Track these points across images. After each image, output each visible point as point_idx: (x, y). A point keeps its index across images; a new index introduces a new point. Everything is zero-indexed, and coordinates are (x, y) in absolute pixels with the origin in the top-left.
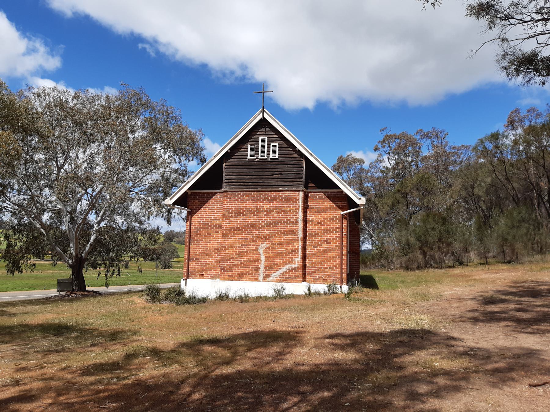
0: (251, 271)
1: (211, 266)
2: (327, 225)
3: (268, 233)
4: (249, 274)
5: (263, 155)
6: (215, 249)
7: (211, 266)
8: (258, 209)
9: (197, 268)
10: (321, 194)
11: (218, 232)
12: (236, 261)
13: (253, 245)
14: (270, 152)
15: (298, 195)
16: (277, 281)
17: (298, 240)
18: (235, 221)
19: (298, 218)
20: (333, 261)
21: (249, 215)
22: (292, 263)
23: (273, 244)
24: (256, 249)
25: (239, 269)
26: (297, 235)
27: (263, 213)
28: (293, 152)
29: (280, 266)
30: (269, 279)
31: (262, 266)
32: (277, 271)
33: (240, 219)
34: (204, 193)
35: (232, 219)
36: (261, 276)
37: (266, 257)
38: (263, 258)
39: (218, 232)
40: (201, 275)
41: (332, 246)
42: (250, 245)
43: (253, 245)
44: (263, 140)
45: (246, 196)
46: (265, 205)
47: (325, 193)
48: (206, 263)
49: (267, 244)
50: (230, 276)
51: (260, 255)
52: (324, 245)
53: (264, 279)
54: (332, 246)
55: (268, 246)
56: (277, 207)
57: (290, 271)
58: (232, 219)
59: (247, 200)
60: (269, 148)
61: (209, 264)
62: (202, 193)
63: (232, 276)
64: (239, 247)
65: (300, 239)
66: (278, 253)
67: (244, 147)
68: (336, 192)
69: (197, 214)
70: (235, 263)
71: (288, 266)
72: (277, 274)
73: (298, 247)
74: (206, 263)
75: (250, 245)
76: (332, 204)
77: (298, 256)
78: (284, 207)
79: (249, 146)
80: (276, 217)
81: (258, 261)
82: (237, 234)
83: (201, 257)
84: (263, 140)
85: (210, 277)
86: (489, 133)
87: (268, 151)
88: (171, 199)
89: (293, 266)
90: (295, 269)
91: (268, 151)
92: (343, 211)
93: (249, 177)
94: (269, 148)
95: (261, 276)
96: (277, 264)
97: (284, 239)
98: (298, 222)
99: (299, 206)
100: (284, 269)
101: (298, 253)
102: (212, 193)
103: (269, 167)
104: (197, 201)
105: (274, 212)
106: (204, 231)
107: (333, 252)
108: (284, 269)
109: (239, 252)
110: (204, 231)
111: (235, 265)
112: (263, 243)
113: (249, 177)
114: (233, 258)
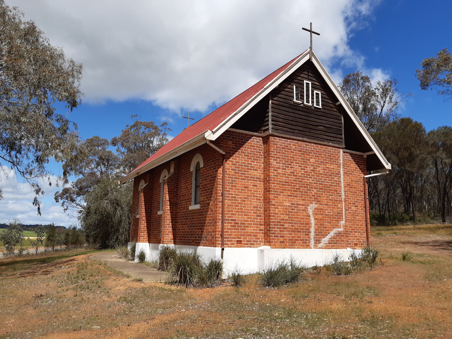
0: (303, 236)
1: (250, 230)
2: (355, 188)
3: (315, 190)
4: (301, 240)
5: (308, 101)
6: (254, 207)
7: (250, 230)
8: (305, 161)
9: (234, 233)
10: (348, 154)
11: (256, 186)
12: (286, 223)
13: (303, 205)
14: (313, 100)
15: (339, 152)
16: (327, 247)
17: (342, 201)
18: (283, 174)
19: (340, 177)
20: (361, 225)
21: (296, 167)
22: (337, 226)
23: (321, 204)
24: (305, 210)
25: (290, 234)
26: (340, 196)
27: (310, 168)
28: (333, 106)
29: (328, 230)
30: (320, 245)
31: (312, 230)
32: (326, 235)
33: (288, 171)
34: (239, 133)
35: (280, 171)
36: (312, 242)
37: (315, 219)
38: (313, 221)
39: (256, 186)
40: (239, 242)
41: (359, 209)
42: (300, 205)
43: (303, 205)
44: (307, 84)
45: (293, 145)
46: (311, 158)
47: (351, 154)
48: (244, 226)
49: (316, 204)
50: (281, 242)
51: (309, 216)
52: (353, 208)
53: (316, 247)
54: (359, 209)
55: (316, 206)
56: (322, 162)
57: (337, 236)
58: (280, 171)
59: (294, 150)
60: (313, 95)
61: (248, 227)
62: (236, 133)
63: (283, 242)
64: (289, 206)
65: (343, 200)
66: (326, 215)
67: (289, 86)
68: (360, 155)
69: (231, 159)
70: (286, 225)
71: (335, 231)
72: (326, 240)
73: (342, 209)
74: (244, 226)
75: (300, 205)
76: (357, 167)
77: (343, 219)
78: (328, 163)
79: (295, 87)
80: (321, 174)
81: (308, 224)
82: (285, 190)
83: (239, 218)
84: (307, 84)
85: (251, 244)
86: (444, 125)
87: (313, 98)
88: (214, 133)
89: (340, 230)
90: (341, 233)
91: (313, 98)
92: (365, 174)
93: (294, 123)
94: (313, 95)
95: (312, 242)
96: (326, 227)
97: (330, 200)
98: (340, 182)
99: (340, 165)
100: (332, 234)
101: (342, 216)
102: (247, 135)
103: (313, 116)
104: (230, 143)
105: (320, 168)
106: (240, 183)
107: (360, 216)
108: (332, 234)
109: (289, 212)
110: (240, 183)
111: (286, 228)
112: (312, 203)
113: (294, 123)
114: (283, 220)
